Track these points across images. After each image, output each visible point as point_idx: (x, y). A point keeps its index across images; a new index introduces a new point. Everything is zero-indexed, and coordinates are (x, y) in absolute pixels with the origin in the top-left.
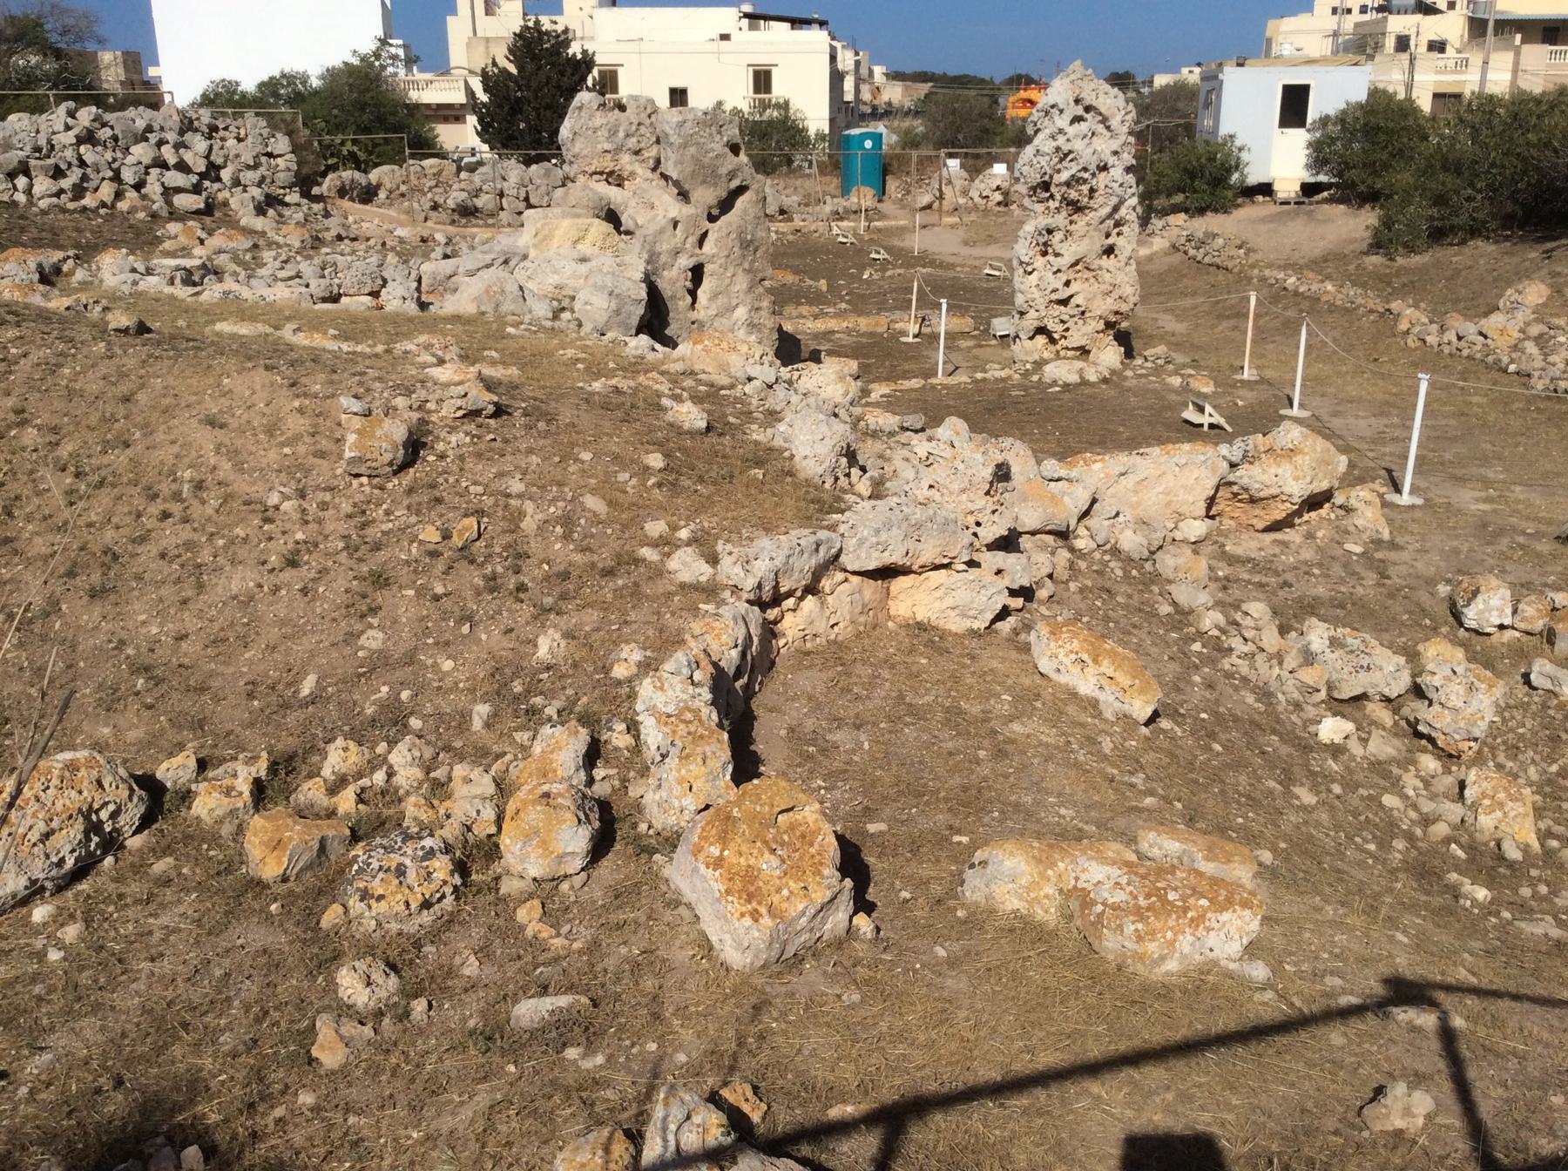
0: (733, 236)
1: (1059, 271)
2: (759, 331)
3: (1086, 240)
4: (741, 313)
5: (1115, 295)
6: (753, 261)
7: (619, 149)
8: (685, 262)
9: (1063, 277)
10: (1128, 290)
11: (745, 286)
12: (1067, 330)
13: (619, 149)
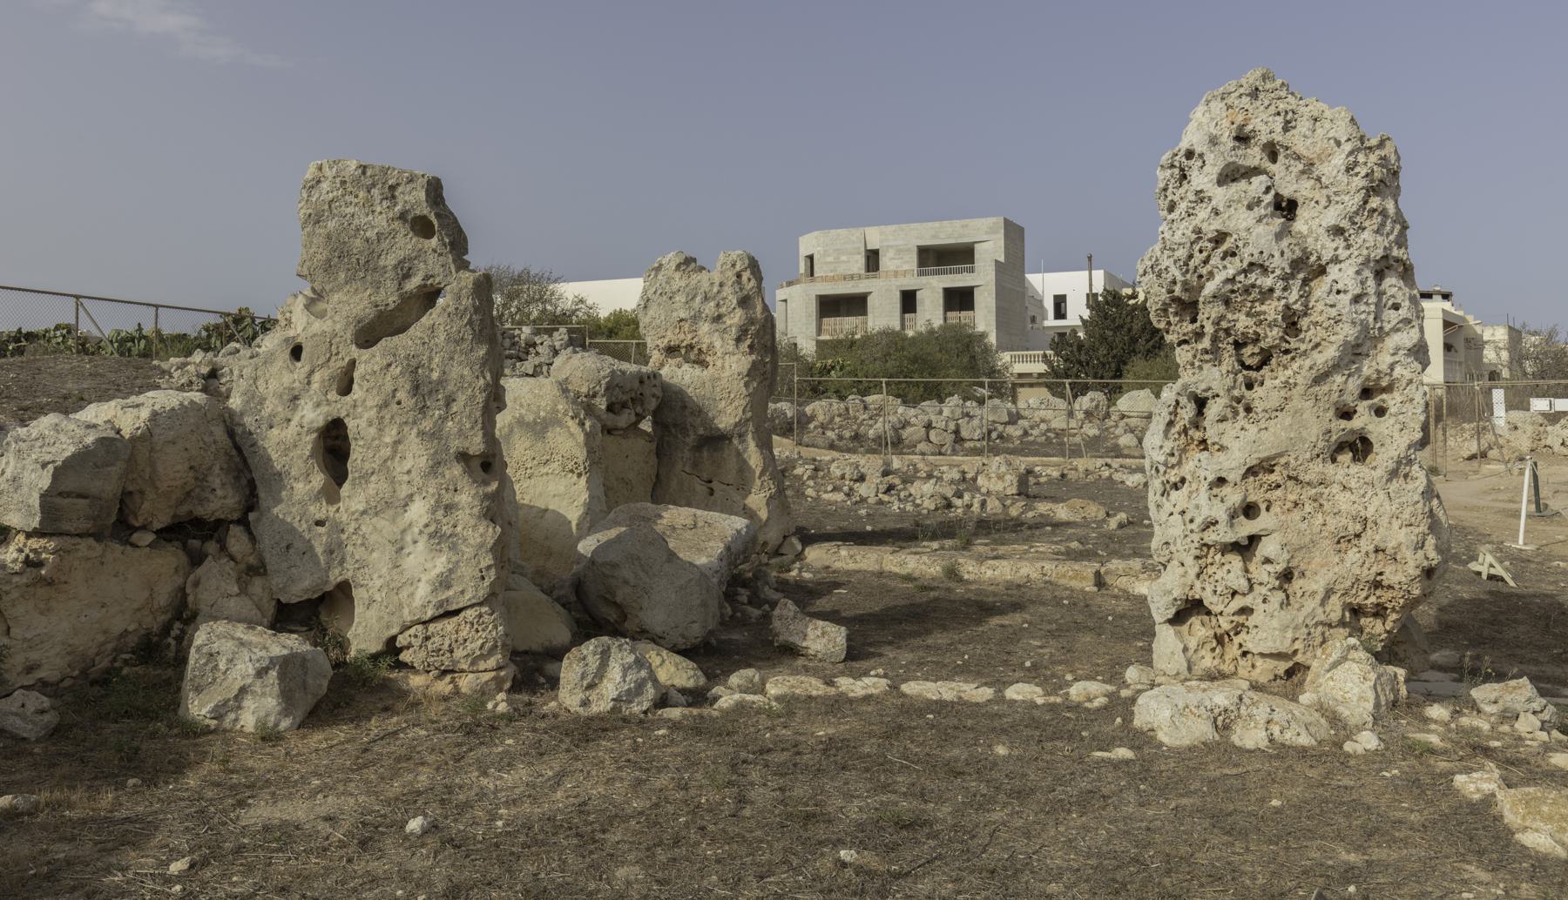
0: (396, 370)
1: (1221, 481)
2: (453, 548)
3: (1285, 419)
4: (418, 511)
5: (1366, 544)
6: (443, 419)
7: (696, 318)
8: (312, 415)
9: (1234, 497)
10: (1398, 536)
11: (423, 462)
12: (1246, 611)
13: (696, 318)
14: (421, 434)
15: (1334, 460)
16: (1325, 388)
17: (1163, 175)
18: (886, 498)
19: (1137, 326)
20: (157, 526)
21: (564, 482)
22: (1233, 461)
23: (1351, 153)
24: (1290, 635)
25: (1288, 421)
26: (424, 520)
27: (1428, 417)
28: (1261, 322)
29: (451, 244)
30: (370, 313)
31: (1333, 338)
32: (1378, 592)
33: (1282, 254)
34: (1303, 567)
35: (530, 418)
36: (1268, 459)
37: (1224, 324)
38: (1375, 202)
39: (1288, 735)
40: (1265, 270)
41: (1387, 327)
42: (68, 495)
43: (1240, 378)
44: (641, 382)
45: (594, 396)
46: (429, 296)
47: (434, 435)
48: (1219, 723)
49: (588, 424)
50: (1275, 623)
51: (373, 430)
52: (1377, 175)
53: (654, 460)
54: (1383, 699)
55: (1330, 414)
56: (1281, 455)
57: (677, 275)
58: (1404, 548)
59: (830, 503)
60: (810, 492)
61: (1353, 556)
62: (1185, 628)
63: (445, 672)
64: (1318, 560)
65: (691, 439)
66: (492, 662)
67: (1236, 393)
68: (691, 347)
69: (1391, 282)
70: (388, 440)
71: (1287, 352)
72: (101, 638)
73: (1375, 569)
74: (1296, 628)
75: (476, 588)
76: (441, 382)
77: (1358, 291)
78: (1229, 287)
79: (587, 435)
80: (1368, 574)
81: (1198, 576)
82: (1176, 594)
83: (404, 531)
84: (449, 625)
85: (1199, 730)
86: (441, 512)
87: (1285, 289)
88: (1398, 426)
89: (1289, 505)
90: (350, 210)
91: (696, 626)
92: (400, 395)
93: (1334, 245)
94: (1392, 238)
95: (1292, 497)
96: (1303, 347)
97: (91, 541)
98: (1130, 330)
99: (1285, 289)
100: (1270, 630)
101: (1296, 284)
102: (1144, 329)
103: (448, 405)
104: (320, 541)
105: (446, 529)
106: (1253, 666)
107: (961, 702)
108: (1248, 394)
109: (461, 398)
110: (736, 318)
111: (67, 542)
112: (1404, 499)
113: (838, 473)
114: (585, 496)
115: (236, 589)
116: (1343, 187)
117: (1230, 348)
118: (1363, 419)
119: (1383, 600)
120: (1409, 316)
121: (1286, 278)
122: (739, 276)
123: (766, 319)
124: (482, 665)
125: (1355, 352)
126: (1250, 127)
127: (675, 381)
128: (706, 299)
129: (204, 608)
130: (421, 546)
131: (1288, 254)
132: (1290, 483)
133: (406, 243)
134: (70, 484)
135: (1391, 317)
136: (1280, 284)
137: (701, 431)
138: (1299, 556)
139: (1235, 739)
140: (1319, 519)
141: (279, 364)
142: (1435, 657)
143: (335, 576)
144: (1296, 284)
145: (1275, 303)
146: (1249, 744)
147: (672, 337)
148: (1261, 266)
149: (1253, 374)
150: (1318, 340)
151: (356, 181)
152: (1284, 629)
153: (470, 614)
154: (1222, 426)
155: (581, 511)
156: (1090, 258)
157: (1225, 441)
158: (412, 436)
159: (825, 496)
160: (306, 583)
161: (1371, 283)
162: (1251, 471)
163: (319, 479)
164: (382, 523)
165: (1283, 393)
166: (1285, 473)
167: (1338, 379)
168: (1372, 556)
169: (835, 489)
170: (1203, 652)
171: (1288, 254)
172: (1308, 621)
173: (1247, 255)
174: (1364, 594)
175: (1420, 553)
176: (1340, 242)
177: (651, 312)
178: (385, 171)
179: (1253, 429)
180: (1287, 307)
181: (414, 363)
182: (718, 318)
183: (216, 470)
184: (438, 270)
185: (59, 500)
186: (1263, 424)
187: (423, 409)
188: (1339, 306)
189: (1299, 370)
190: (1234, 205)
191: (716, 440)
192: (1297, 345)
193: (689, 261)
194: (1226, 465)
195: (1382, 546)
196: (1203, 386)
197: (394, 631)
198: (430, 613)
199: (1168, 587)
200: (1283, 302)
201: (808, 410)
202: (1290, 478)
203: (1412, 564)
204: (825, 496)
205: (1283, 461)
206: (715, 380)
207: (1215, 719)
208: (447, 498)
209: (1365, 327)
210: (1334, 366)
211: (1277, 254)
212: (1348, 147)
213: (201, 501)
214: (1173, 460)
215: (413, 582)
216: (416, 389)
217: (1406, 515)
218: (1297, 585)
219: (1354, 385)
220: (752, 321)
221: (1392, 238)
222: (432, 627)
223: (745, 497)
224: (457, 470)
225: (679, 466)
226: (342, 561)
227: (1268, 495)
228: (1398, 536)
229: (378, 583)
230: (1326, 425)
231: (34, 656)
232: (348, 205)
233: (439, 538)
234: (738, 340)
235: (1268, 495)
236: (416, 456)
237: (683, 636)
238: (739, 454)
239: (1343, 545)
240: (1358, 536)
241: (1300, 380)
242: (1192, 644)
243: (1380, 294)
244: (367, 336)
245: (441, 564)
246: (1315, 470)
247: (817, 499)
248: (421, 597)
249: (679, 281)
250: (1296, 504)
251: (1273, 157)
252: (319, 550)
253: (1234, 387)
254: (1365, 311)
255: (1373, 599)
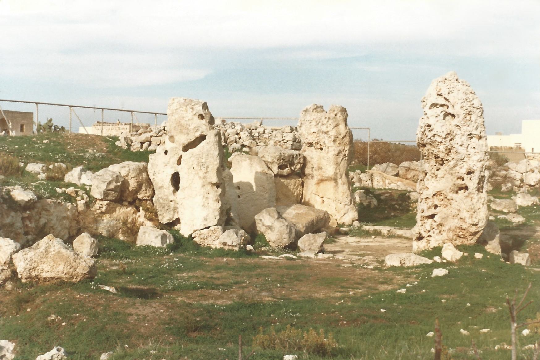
5: (459, 217)
37: (430, 151)
42: (108, 190)
46: (203, 138)
65: (315, 180)
67: (433, 171)
86: (204, 199)
109: (211, 167)
163: (172, 189)
179: (435, 183)
224: (209, 187)
244: (186, 148)
246: (451, 195)
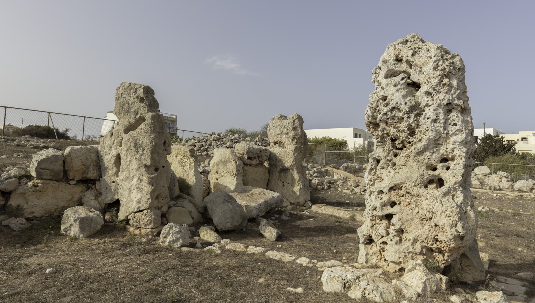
2: (141, 192)
3: (405, 169)
6: (142, 155)
7: (282, 133)
8: (114, 152)
9: (385, 198)
11: (136, 167)
13: (282, 133)
14: (136, 159)
15: (426, 187)
16: (422, 157)
17: (373, 77)
18: (363, 193)
19: (498, 146)
20: (76, 179)
21: (231, 178)
22: (384, 185)
23: (436, 61)
24: (397, 255)
25: (407, 170)
26: (135, 184)
27: (78, 143)
28: (399, 131)
29: (149, 105)
30: (128, 124)
31: (424, 137)
32: (438, 243)
33: (406, 103)
34: (407, 228)
35: (223, 160)
36: (399, 184)
37: (385, 132)
38: (446, 81)
39: (371, 296)
40: (400, 110)
41: (451, 133)
42: (41, 168)
43: (392, 152)
44: (261, 151)
45: (244, 154)
47: (139, 159)
48: (347, 285)
49: (238, 162)
50: (393, 250)
51: (125, 157)
52: (447, 70)
53: (267, 175)
54: (429, 289)
55: (424, 168)
56: (403, 183)
57: (278, 121)
58: (446, 226)
59: (345, 193)
60: (339, 189)
61: (427, 227)
62: (370, 246)
63: (139, 228)
64: (413, 226)
65: (278, 169)
66: (150, 227)
67: (388, 158)
68: (281, 142)
69: (454, 116)
70: (128, 160)
71: (410, 143)
72: (56, 207)
73: (434, 233)
74: (400, 253)
75: (146, 204)
76: (142, 144)
77: (434, 117)
78: (385, 117)
79: (237, 166)
80: (431, 235)
81: (371, 227)
82: (364, 233)
83: (131, 186)
84: (140, 214)
85: (337, 287)
86: (139, 181)
87: (408, 117)
88: (453, 175)
89: (407, 203)
90: (125, 96)
91: (228, 224)
92: (132, 147)
93: (427, 99)
94: (454, 96)
95: (408, 200)
96: (415, 141)
97: (55, 182)
98: (495, 147)
99: (408, 117)
100: (392, 252)
101: (413, 115)
102: (500, 147)
103: (143, 151)
104: (113, 186)
105: (140, 187)
106: (388, 265)
107: (280, 261)
108: (394, 159)
110: (292, 134)
111: (46, 181)
112: (448, 205)
113: (349, 184)
114: (236, 183)
115: (94, 198)
116: (432, 75)
117: (390, 141)
118: (441, 172)
119: (439, 247)
120: (461, 128)
121: (408, 113)
122: (294, 121)
123: (302, 134)
124: (148, 227)
125: (436, 143)
126: (401, 55)
127: (274, 152)
128: (284, 128)
129: (85, 202)
130: (135, 191)
131: (409, 104)
132: (407, 195)
133: (137, 104)
134: (43, 166)
135: (452, 129)
136: (406, 116)
137: (281, 167)
138: (406, 224)
139: (349, 294)
140: (416, 210)
141: (108, 138)
142: (521, 274)
143: (116, 197)
144: (413, 115)
145: (405, 123)
146: (353, 296)
147: (276, 139)
148: (398, 108)
149: (397, 151)
150: (420, 138)
151: (128, 88)
152: (396, 252)
153: (145, 212)
154: (382, 170)
155: (234, 187)
156: (484, 124)
157: (383, 176)
158: (134, 160)
159: (344, 191)
160: (109, 198)
161: (442, 116)
162: (391, 189)
164: (126, 183)
165: (406, 158)
166: (406, 190)
167: (428, 154)
168: (434, 227)
169: (347, 189)
170: (374, 257)
171: (408, 103)
172: (405, 251)
173: (392, 104)
174: (430, 243)
175: (454, 229)
176: (430, 98)
177: (271, 132)
178: (135, 84)
179: (393, 172)
180: (410, 125)
181: (136, 138)
182: (287, 134)
183: (92, 166)
184: (143, 112)
185: (41, 170)
186: (397, 171)
187: (137, 152)
188: (427, 124)
189: (411, 150)
190: (389, 85)
191: (285, 170)
192: (412, 140)
193: (281, 116)
194: (382, 186)
195: (437, 224)
196: (377, 155)
197: (128, 214)
198: (135, 210)
199: (363, 230)
200: (408, 123)
201: (364, 166)
202: (408, 193)
203: (449, 233)
204: (344, 191)
205: (404, 185)
206: (285, 152)
207: (345, 284)
208: (141, 177)
209: (438, 132)
210: (425, 148)
211: (403, 104)
212: (434, 59)
213: (88, 174)
214: (371, 183)
215: (132, 201)
216: (136, 146)
217: (448, 212)
218: (404, 236)
219: (436, 157)
220: (297, 135)
221: (454, 96)
222: (136, 214)
223: (293, 188)
225: (275, 177)
226: (118, 193)
227: (399, 199)
228: (443, 220)
229: (125, 200)
230: (422, 172)
231: (33, 210)
232: (125, 94)
233: (139, 189)
234: (293, 140)
235: (399, 199)
236: (134, 165)
237: (224, 226)
238: (292, 175)
239: (424, 222)
240: (431, 219)
241: (412, 154)
242: (371, 252)
243: (447, 120)
244: (127, 131)
245: (139, 196)
246: (416, 190)
247: (341, 192)
248: (134, 206)
249: (279, 122)
250: (410, 204)
251: (411, 66)
252: (113, 189)
253: (388, 156)
254: (439, 126)
255: (435, 246)
